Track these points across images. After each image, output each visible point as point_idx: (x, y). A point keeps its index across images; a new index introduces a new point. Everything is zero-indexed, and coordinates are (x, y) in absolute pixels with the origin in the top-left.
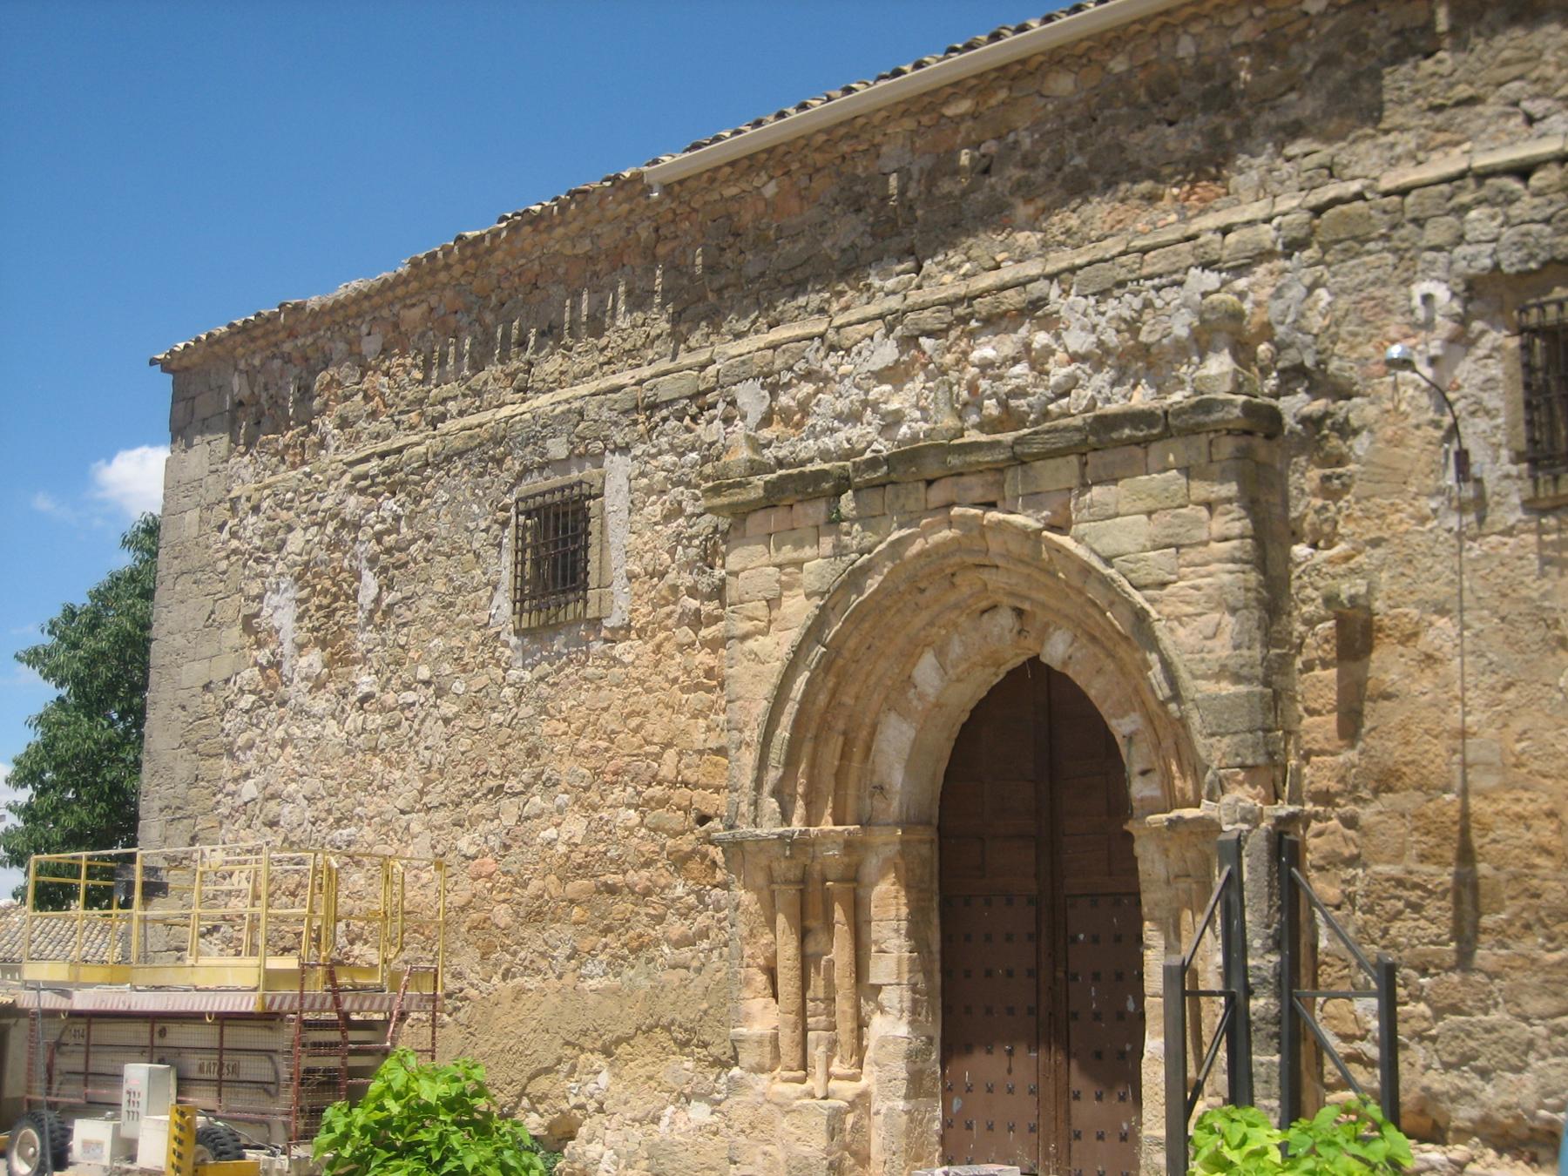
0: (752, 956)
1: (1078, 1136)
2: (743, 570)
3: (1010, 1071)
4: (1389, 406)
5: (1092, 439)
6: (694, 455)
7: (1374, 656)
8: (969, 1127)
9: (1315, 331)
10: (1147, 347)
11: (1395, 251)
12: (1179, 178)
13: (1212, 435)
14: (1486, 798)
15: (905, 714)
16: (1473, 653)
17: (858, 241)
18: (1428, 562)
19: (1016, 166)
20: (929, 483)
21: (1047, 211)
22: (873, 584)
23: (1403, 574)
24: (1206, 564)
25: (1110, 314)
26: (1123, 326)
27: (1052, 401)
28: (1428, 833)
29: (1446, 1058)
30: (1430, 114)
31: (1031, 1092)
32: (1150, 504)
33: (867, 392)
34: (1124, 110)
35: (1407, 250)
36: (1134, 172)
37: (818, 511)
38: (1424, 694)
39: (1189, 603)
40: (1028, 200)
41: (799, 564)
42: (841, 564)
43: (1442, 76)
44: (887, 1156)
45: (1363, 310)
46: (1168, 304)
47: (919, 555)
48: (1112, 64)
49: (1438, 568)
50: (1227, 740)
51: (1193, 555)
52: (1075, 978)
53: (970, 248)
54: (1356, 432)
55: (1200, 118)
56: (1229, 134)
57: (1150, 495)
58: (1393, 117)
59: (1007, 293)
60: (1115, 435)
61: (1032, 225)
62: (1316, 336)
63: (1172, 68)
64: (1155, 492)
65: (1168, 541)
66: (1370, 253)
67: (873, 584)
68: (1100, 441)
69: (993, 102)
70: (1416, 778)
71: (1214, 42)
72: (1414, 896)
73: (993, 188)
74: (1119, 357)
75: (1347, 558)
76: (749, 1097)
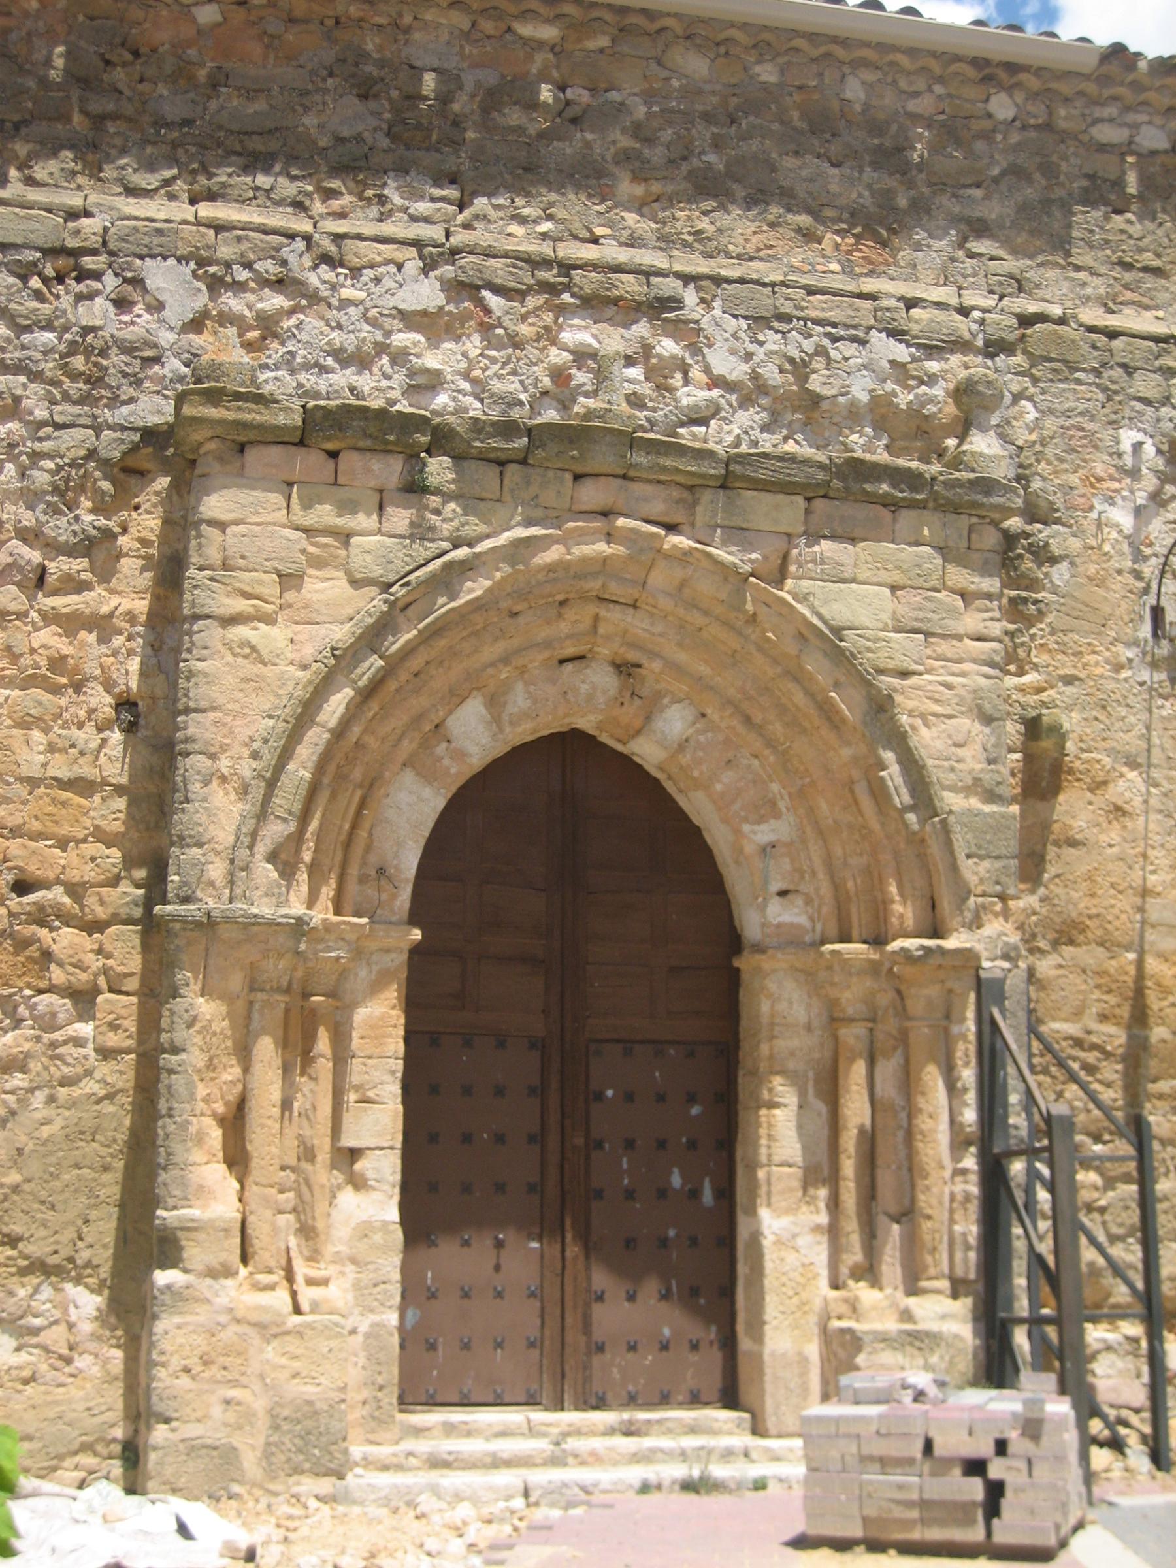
0: (207, 1100)
1: (601, 1348)
2: (237, 523)
3: (497, 1268)
4: (1093, 543)
5: (836, 483)
6: (49, 337)
7: (1061, 798)
8: (432, 1347)
9: (1020, 443)
10: (816, 400)
11: (1105, 389)
12: (845, 226)
13: (974, 520)
14: (1166, 960)
15: (429, 776)
16: (1160, 811)
17: (366, 134)
18: (1123, 711)
19: (624, 131)
20: (577, 477)
21: (671, 200)
22: (474, 589)
23: (1096, 719)
24: (959, 661)
25: (770, 346)
26: (788, 367)
27: (683, 424)
28: (1109, 992)
29: (1115, 1230)
30: (1118, 268)
31: (532, 1295)
32: (896, 577)
33: (388, 334)
34: (776, 126)
35: (1116, 392)
36: (790, 199)
37: (391, 470)
38: (1111, 846)
39: (937, 701)
40: (636, 178)
41: (345, 537)
42: (421, 551)
43: (1130, 237)
44: (366, 1393)
45: (1071, 438)
46: (846, 359)
47: (551, 568)
48: (757, 69)
49: (1132, 719)
50: (986, 864)
51: (944, 647)
52: (599, 1145)
53: (551, 205)
54: (1054, 560)
55: (869, 174)
56: (902, 202)
57: (898, 568)
58: (1082, 256)
59: (624, 277)
60: (868, 487)
61: (641, 206)
62: (1020, 448)
63: (835, 105)
64: (905, 566)
65: (916, 625)
66: (1079, 382)
67: (474, 589)
68: (847, 489)
69: (591, 45)
70: (1099, 932)
71: (889, 100)
72: (1091, 1057)
73: (588, 145)
74: (775, 400)
75: (1039, 690)
76: (201, 1316)
